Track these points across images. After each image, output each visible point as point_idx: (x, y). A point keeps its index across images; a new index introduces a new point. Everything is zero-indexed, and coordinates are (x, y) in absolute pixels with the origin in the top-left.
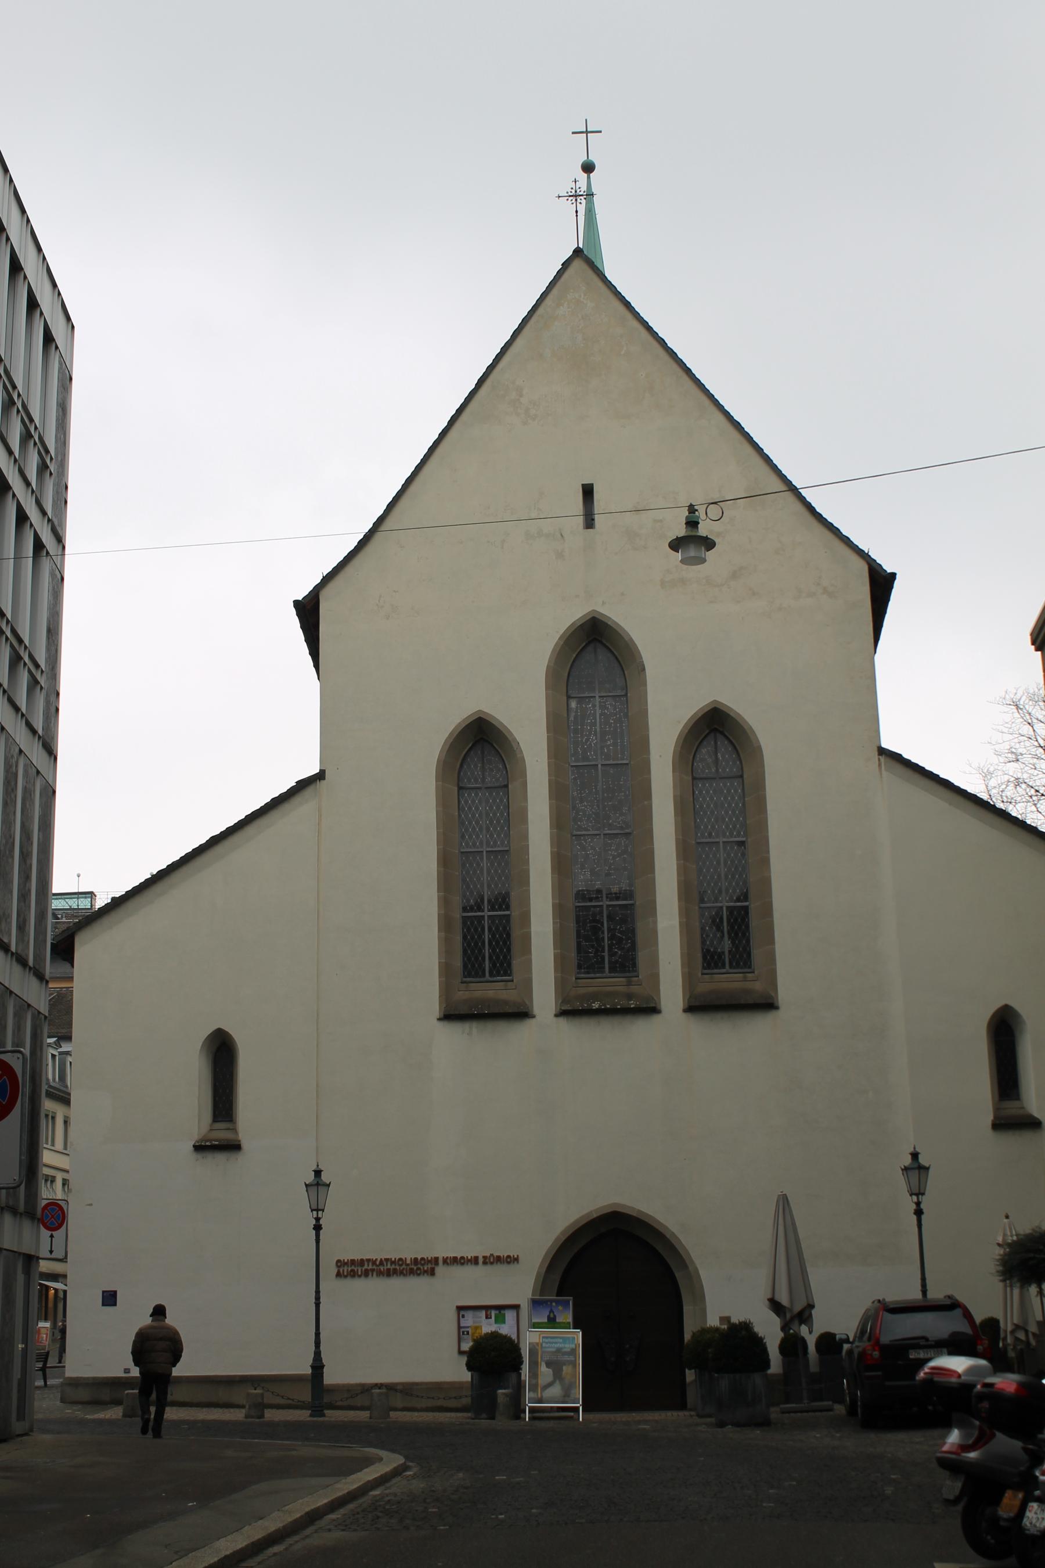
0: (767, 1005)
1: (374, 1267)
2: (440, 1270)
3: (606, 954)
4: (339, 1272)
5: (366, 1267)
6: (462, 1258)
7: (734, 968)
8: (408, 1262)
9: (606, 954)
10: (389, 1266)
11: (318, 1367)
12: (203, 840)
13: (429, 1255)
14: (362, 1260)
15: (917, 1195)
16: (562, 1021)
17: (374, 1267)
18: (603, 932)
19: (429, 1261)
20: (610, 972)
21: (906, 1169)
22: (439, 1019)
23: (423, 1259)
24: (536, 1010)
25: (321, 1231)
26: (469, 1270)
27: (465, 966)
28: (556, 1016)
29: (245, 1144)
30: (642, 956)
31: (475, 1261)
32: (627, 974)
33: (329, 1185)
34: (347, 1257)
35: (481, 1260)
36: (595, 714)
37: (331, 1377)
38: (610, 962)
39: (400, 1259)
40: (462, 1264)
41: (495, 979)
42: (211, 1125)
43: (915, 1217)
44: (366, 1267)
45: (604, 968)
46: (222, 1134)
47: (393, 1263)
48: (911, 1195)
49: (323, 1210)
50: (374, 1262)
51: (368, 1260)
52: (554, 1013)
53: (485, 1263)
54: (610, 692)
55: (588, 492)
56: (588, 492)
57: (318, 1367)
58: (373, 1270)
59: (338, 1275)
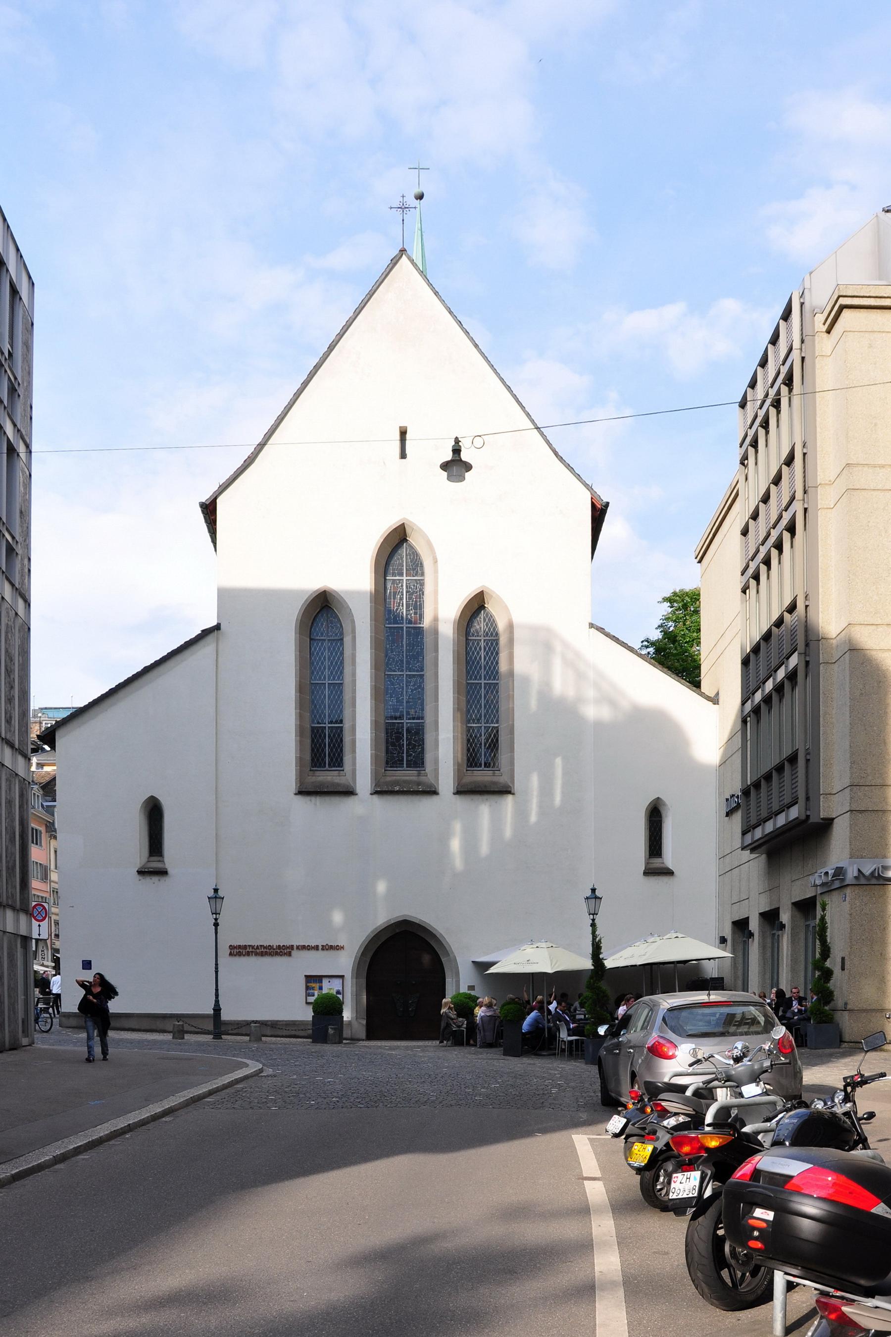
0: (505, 791)
1: (253, 950)
2: (294, 953)
3: (405, 755)
4: (231, 952)
5: (248, 950)
6: (309, 946)
7: (488, 767)
8: (275, 947)
9: (405, 755)
10: (262, 950)
11: (217, 1009)
12: (139, 669)
13: (288, 943)
14: (245, 945)
15: (593, 914)
16: (375, 798)
17: (253, 950)
18: (403, 741)
19: (288, 948)
20: (407, 767)
21: (587, 898)
22: (454, 794)
23: (284, 946)
24: (358, 790)
25: (219, 927)
26: (313, 953)
27: (313, 760)
28: (454, 794)
29: (170, 871)
30: (428, 757)
31: (316, 948)
32: (418, 769)
33: (223, 898)
34: (235, 944)
35: (320, 947)
36: (402, 592)
37: (225, 1016)
38: (407, 761)
39: (270, 946)
40: (309, 950)
41: (331, 769)
42: (148, 859)
43: (214, 927)
44: (248, 950)
45: (403, 764)
46: (155, 865)
47: (265, 947)
48: (213, 914)
49: (219, 914)
50: (253, 947)
51: (249, 946)
52: (370, 792)
53: (323, 949)
54: (413, 576)
55: (403, 433)
56: (403, 433)
57: (217, 1009)
58: (252, 952)
59: (231, 954)
